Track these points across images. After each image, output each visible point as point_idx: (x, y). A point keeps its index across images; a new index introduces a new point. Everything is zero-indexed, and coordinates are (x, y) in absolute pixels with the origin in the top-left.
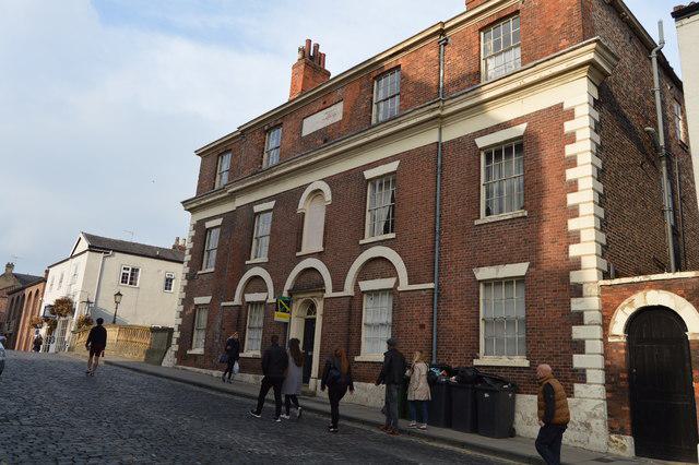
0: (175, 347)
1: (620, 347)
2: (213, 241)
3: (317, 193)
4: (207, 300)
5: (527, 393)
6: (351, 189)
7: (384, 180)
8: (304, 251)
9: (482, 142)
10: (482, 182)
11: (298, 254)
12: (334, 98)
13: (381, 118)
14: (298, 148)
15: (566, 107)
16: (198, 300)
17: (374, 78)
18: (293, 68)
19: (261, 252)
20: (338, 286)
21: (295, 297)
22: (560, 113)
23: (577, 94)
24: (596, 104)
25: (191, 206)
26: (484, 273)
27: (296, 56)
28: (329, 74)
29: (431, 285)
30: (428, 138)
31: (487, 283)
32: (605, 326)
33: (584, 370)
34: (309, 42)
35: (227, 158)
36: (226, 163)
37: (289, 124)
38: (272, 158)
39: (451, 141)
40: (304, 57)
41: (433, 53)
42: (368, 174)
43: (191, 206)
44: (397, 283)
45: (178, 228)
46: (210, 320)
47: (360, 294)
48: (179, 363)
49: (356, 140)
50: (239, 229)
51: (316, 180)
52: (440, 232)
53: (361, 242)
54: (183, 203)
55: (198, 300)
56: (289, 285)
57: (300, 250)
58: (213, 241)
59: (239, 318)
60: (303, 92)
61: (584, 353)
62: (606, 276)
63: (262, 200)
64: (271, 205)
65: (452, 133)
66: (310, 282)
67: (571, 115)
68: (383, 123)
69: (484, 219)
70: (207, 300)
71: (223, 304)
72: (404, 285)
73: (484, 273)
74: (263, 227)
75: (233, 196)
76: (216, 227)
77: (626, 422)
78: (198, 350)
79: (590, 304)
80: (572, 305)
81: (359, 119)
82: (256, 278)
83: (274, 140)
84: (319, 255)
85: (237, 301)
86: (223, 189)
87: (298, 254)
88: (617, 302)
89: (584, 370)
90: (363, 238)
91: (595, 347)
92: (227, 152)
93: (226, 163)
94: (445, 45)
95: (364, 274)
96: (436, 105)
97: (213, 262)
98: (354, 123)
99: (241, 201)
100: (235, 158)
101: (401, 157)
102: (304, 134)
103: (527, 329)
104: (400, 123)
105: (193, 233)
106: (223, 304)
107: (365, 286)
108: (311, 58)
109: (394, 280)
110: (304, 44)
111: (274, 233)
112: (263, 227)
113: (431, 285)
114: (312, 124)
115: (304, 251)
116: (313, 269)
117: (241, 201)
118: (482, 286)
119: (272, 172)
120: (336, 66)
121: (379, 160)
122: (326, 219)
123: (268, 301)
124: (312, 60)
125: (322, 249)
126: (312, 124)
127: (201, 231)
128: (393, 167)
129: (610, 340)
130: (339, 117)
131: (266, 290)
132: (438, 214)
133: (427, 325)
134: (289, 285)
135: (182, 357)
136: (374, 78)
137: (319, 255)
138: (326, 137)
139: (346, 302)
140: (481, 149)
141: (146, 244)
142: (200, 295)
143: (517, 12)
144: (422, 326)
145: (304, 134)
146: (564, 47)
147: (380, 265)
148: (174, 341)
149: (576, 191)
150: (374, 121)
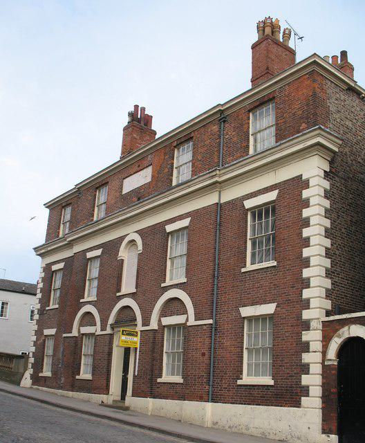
0: (30, 371)
1: (332, 369)
2: (57, 282)
3: (132, 242)
4: (52, 331)
5: (272, 405)
6: (156, 239)
7: (259, 212)
8: (168, 282)
9: (248, 204)
10: (248, 237)
11: (118, 294)
12: (146, 163)
13: (259, 150)
14: (119, 204)
15: (304, 178)
16: (47, 332)
17: (175, 147)
18: (252, 48)
19: (91, 294)
20: (146, 322)
21: (116, 330)
22: (300, 183)
23: (313, 170)
24: (327, 175)
25: (42, 252)
26: (246, 311)
27: (125, 120)
28: (154, 133)
29: (210, 321)
30: (210, 200)
31: (250, 319)
32: (324, 353)
33: (308, 387)
34: (136, 107)
35: (69, 210)
36: (67, 214)
37: (114, 183)
38: (98, 214)
39: (228, 203)
40: (133, 120)
41: (215, 128)
42: (169, 228)
43: (42, 252)
44: (187, 320)
45: (31, 271)
46: (55, 349)
47: (162, 327)
48: (34, 383)
49: (153, 202)
50: (75, 269)
51: (131, 232)
52: (218, 278)
53: (163, 285)
54: (34, 249)
55: (47, 332)
56: (111, 320)
57: (119, 290)
58: (57, 282)
59: (77, 343)
60: (122, 158)
61: (308, 374)
62: (328, 313)
63: (91, 247)
64: (98, 252)
65: (229, 195)
66: (126, 318)
67: (306, 184)
68: (182, 184)
69: (249, 267)
70: (52, 331)
71: (64, 335)
72: (192, 322)
73: (246, 311)
74: (94, 271)
75: (70, 245)
76: (60, 270)
77: (334, 426)
78: (46, 372)
79: (313, 336)
80: (303, 337)
81: (162, 181)
82: (88, 313)
83: (102, 197)
84: (132, 295)
85: (75, 333)
86: (64, 238)
87: (118, 294)
88: (332, 334)
89: (308, 387)
90: (49, 306)
91: (316, 369)
92: (68, 205)
93: (67, 214)
94: (224, 122)
95: (165, 312)
96: (214, 173)
97: (94, 291)
98: (160, 184)
99: (78, 248)
100: (72, 208)
101: (193, 215)
102: (124, 192)
103: (274, 356)
104: (189, 187)
105: (43, 275)
106: (64, 335)
107: (167, 321)
108: (139, 121)
109: (186, 316)
110: (132, 109)
111: (101, 277)
112: (94, 271)
113: (210, 321)
114: (132, 183)
115: (168, 282)
116: (128, 307)
117: (78, 248)
118: (166, 329)
119: (99, 225)
120: (162, 127)
121: (176, 217)
122: (138, 266)
123: (189, 324)
124: (139, 123)
125: (135, 291)
126: (132, 183)
127: (49, 273)
128: (272, 196)
129: (326, 363)
130: (149, 179)
131: (185, 312)
132: (217, 263)
133: (207, 353)
134: (111, 320)
135: (36, 379)
136: (175, 147)
137: (132, 295)
138: (139, 195)
139: (151, 335)
140: (248, 210)
141: (277, 182)
142: (48, 328)
143: (274, 98)
144: (203, 354)
145: (124, 192)
146: (303, 130)
147: (176, 303)
148: (30, 366)
149: (309, 246)
150: (174, 183)
